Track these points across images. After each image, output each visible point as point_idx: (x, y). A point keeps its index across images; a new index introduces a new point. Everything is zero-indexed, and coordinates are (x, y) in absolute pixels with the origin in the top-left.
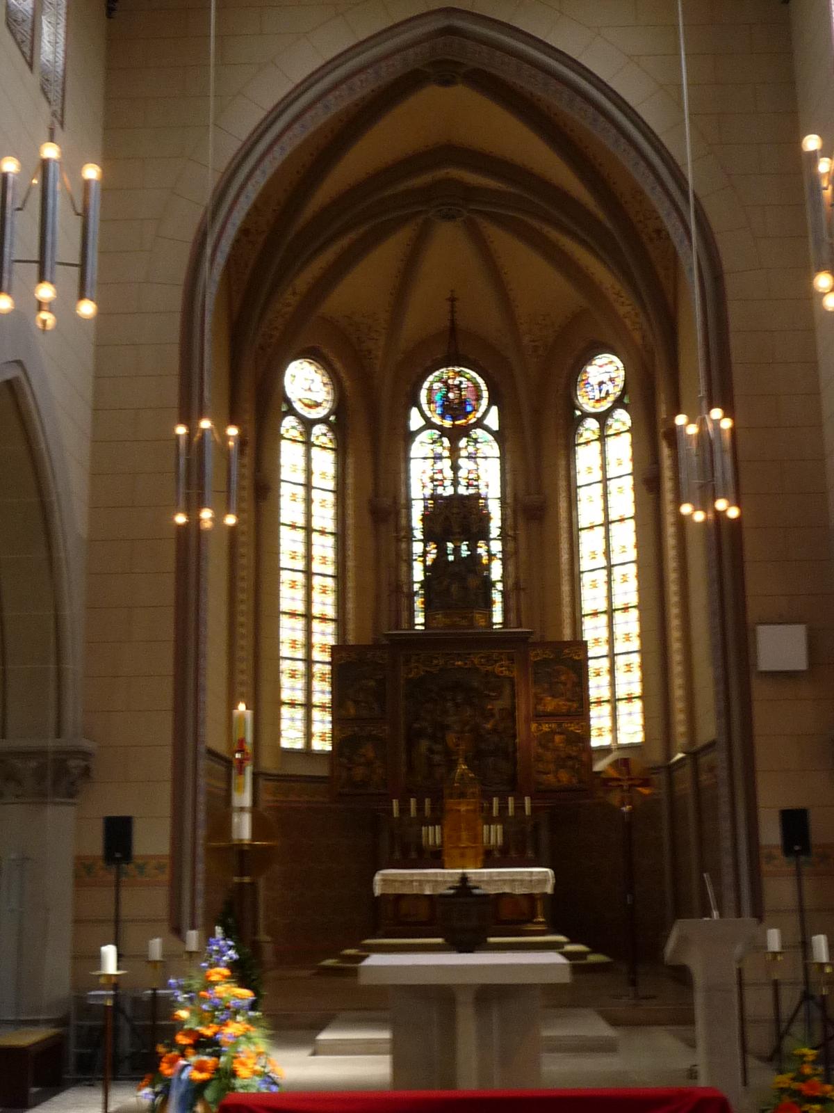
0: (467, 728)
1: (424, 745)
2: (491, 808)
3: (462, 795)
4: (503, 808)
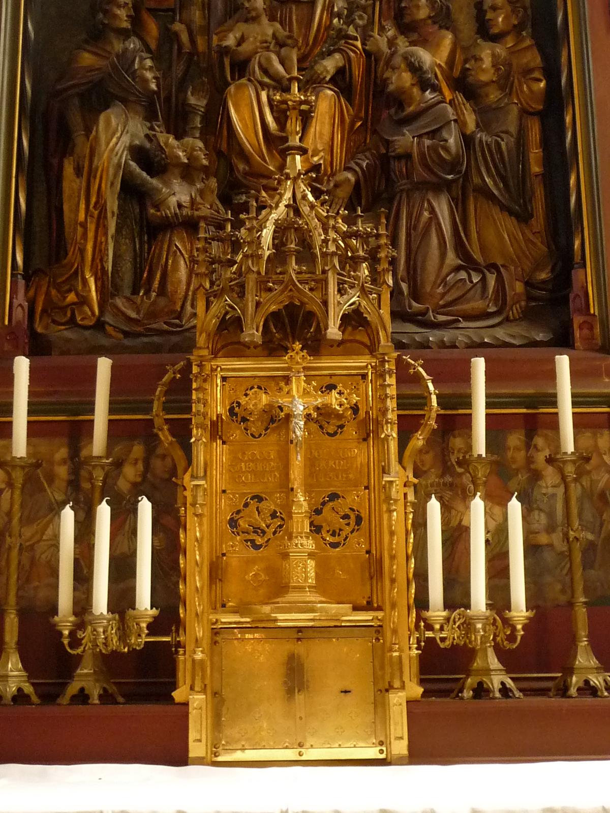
0: (330, 65)
1: (117, 135)
2: (455, 422)
3: (294, 327)
4: (524, 416)
